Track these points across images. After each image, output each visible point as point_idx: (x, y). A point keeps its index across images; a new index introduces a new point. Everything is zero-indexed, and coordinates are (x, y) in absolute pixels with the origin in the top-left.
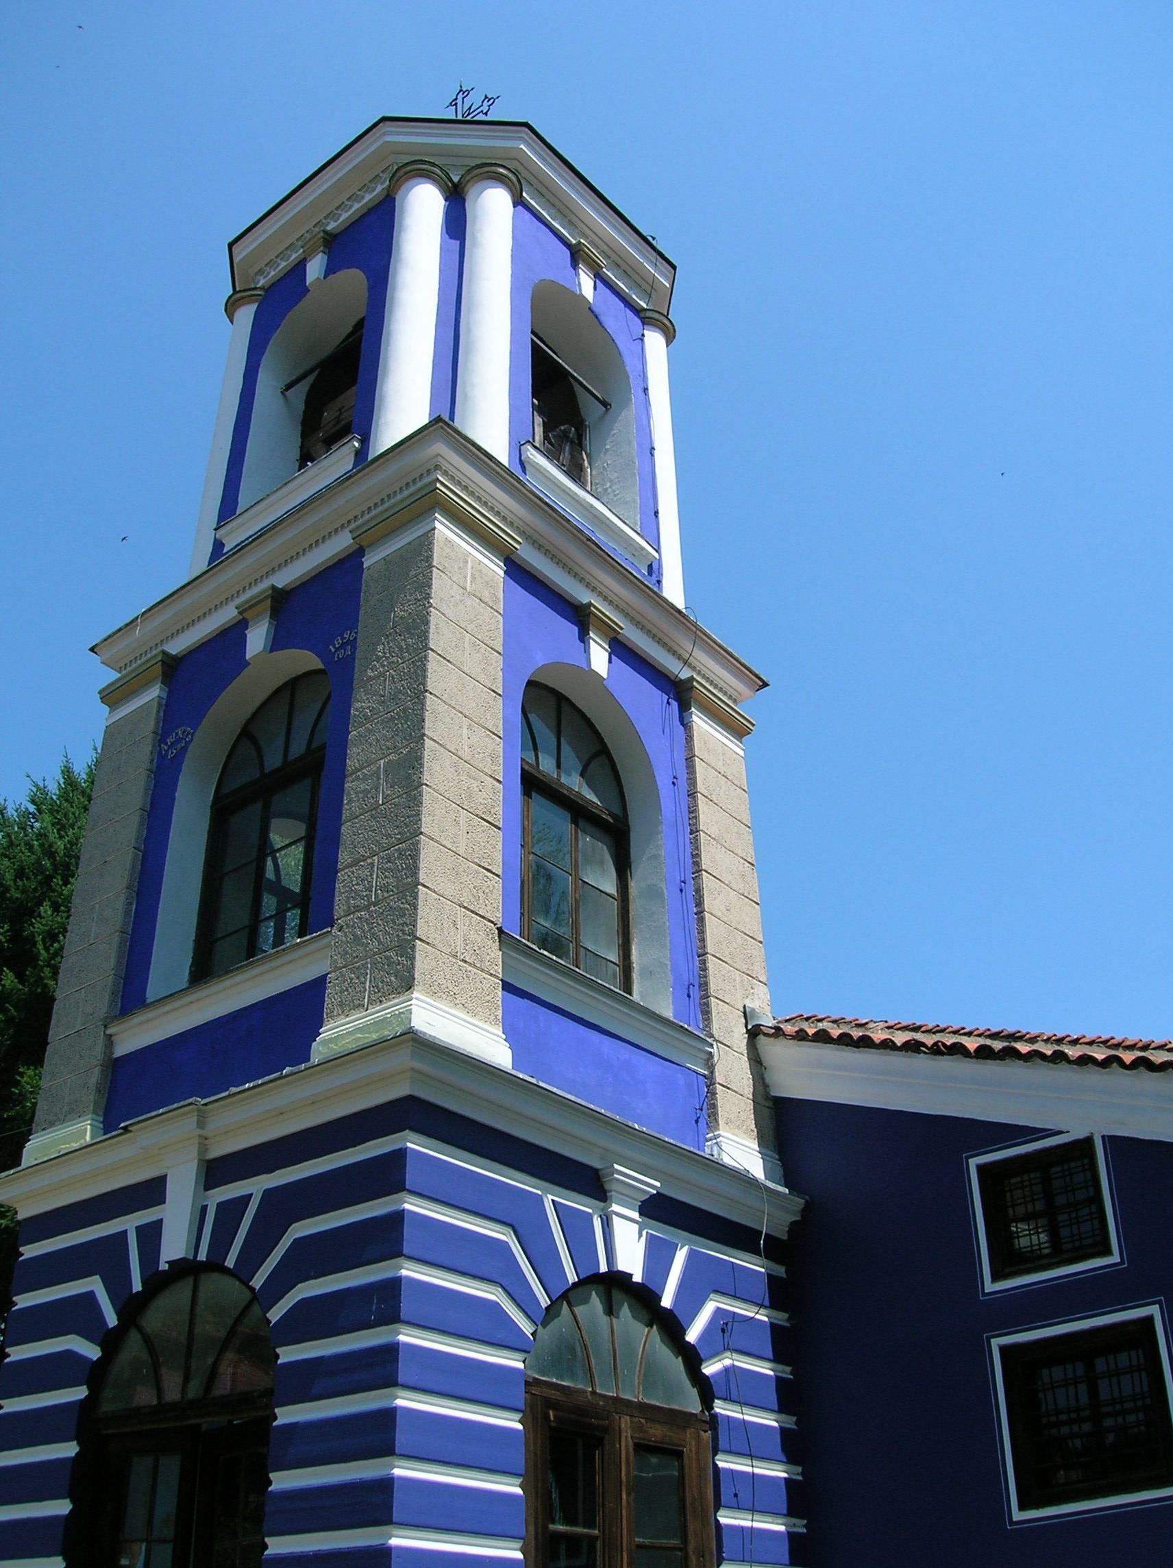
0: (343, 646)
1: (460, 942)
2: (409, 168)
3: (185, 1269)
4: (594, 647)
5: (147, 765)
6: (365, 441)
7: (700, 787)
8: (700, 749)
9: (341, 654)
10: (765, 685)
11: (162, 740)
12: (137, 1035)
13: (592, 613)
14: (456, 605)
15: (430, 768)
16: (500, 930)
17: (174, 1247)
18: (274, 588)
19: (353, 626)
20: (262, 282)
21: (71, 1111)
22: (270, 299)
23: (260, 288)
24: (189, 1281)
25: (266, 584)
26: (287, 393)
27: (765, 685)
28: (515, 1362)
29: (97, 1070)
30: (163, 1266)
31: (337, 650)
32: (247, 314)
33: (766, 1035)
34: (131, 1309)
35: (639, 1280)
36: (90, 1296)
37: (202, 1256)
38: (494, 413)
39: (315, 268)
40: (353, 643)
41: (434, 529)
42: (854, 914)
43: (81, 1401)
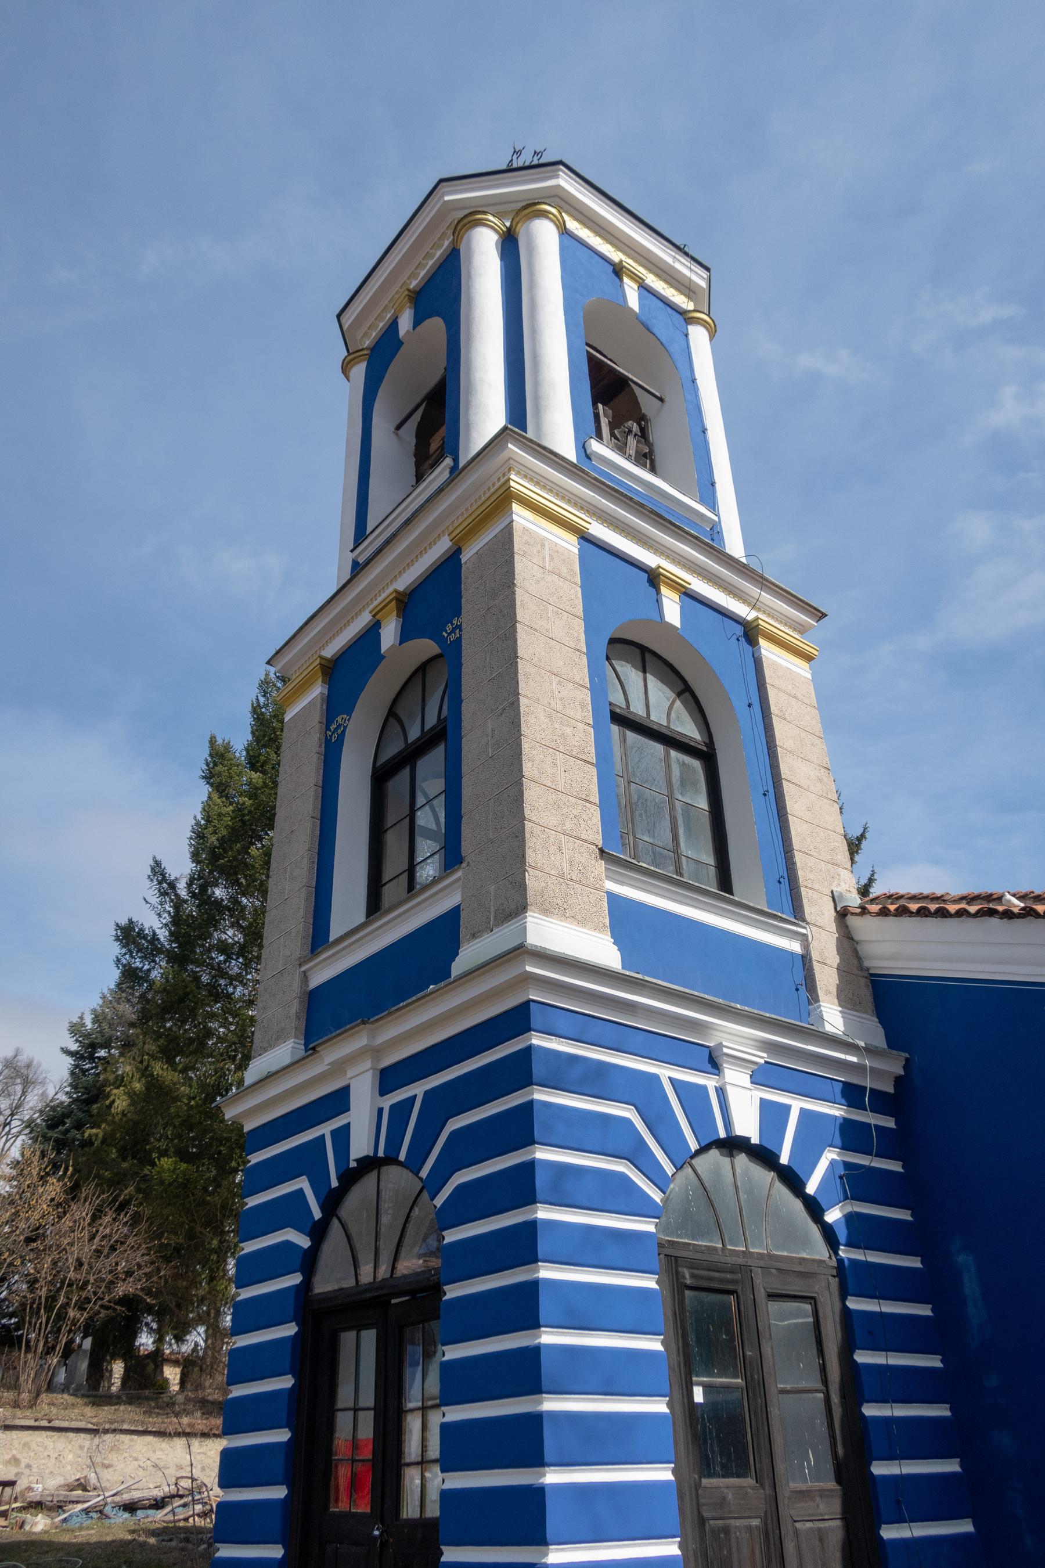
0: (453, 631)
1: (565, 865)
2: (462, 224)
3: (370, 1164)
4: (666, 602)
5: (317, 749)
6: (456, 460)
7: (774, 709)
8: (770, 677)
9: (453, 637)
10: (824, 615)
11: (328, 729)
12: (325, 971)
13: (661, 574)
14: (538, 582)
15: (527, 721)
16: (601, 851)
17: (360, 1147)
18: (396, 591)
19: (458, 613)
20: (367, 343)
21: (277, 1039)
22: (378, 357)
23: (366, 349)
24: (374, 1174)
25: (391, 589)
26: (400, 432)
27: (824, 615)
28: (647, 1226)
29: (296, 1003)
30: (353, 1164)
31: (449, 634)
32: (359, 371)
33: (852, 914)
34: (332, 1202)
35: (757, 1142)
36: (301, 1191)
37: (381, 1154)
38: (559, 421)
39: (405, 324)
40: (459, 627)
41: (512, 521)
42: (873, 819)
43: (297, 1285)
